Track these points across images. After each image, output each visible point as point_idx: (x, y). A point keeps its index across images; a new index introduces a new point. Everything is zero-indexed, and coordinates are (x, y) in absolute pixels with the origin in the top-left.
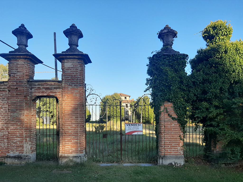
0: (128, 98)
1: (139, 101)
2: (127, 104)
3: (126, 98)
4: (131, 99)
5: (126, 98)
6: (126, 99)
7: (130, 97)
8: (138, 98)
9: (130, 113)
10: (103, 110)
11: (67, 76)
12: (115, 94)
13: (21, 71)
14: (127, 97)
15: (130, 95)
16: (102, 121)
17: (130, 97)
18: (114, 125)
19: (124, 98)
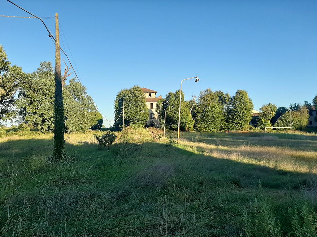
0: (153, 94)
1: (169, 97)
2: (152, 103)
3: (150, 95)
4: (158, 96)
5: (150, 95)
6: (151, 96)
7: (156, 93)
8: (167, 94)
9: (156, 116)
10: (119, 111)
11: (313, 141)
12: (135, 88)
13: (308, 134)
14: (152, 93)
15: (156, 91)
16: (117, 127)
17: (156, 93)
18: (138, 134)
19: (148, 95)
